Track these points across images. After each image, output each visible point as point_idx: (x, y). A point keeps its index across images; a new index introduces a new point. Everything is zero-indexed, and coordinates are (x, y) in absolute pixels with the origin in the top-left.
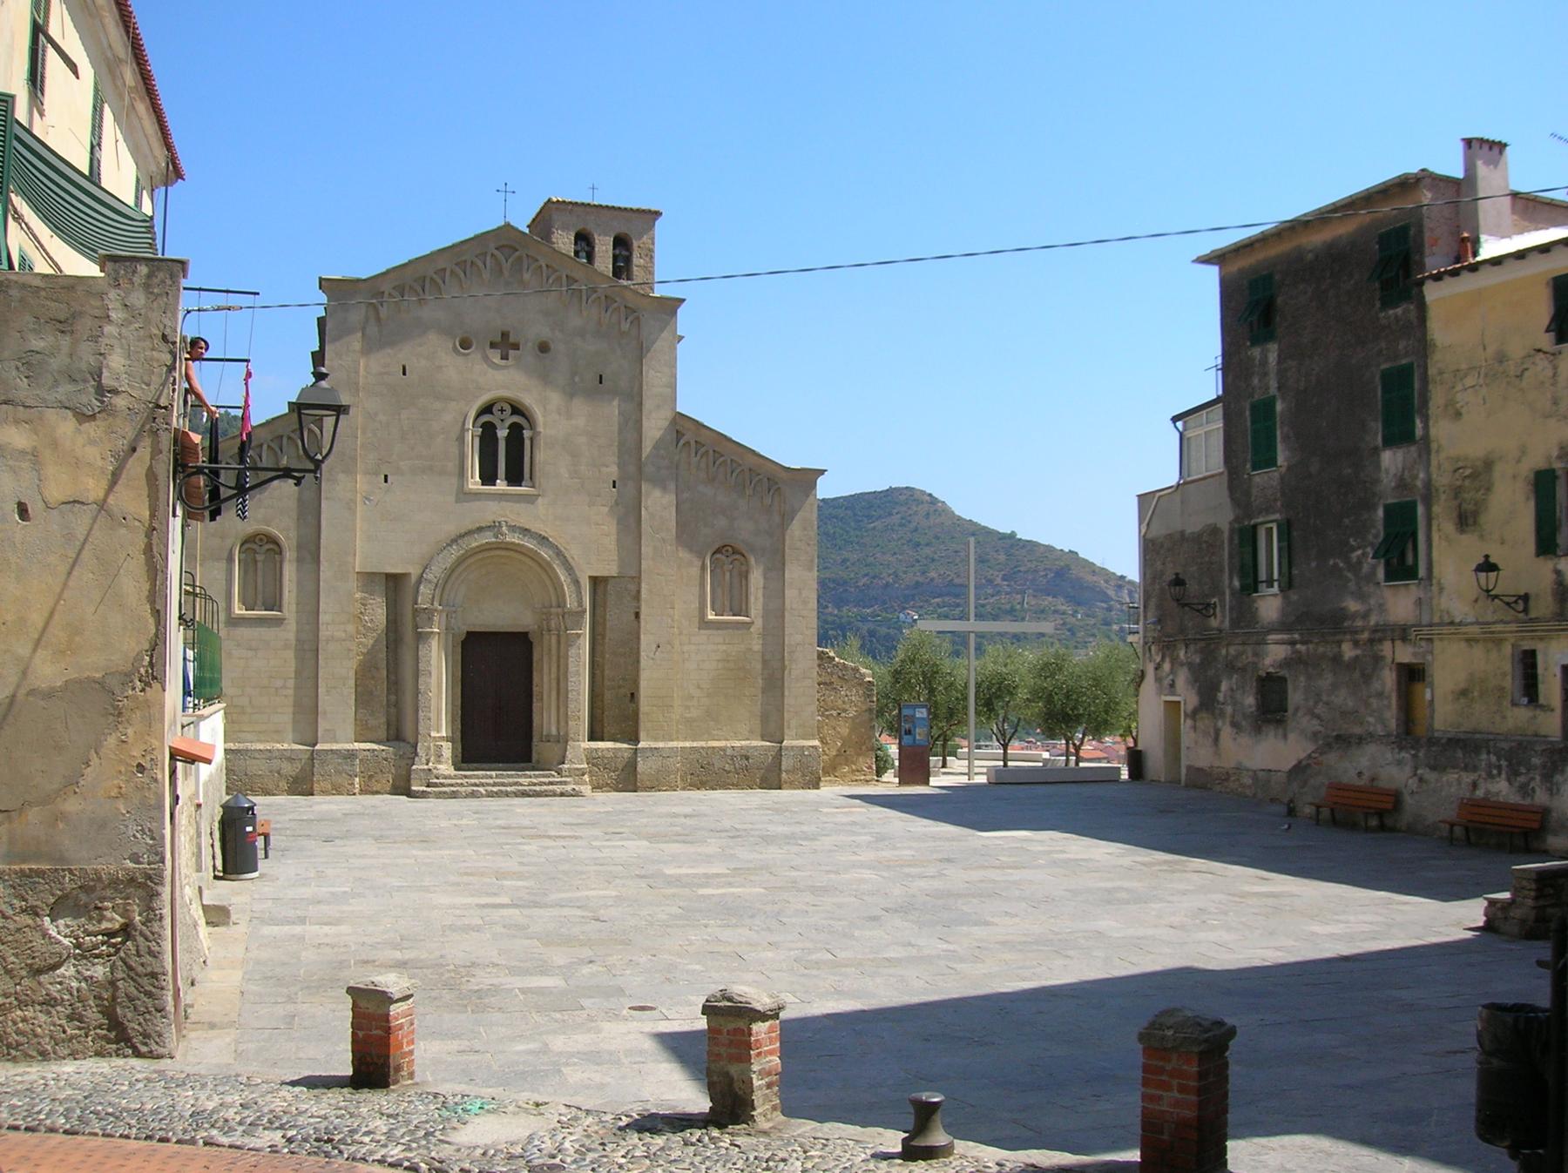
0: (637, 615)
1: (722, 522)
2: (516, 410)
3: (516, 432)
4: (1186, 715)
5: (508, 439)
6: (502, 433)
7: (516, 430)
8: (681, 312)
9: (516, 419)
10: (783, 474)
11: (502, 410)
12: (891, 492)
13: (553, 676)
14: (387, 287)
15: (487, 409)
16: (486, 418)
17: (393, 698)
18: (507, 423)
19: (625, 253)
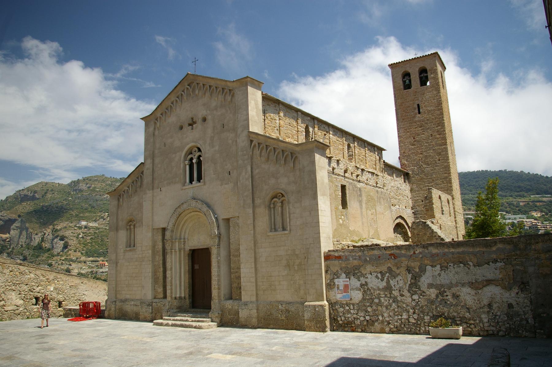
19: (425, 75)
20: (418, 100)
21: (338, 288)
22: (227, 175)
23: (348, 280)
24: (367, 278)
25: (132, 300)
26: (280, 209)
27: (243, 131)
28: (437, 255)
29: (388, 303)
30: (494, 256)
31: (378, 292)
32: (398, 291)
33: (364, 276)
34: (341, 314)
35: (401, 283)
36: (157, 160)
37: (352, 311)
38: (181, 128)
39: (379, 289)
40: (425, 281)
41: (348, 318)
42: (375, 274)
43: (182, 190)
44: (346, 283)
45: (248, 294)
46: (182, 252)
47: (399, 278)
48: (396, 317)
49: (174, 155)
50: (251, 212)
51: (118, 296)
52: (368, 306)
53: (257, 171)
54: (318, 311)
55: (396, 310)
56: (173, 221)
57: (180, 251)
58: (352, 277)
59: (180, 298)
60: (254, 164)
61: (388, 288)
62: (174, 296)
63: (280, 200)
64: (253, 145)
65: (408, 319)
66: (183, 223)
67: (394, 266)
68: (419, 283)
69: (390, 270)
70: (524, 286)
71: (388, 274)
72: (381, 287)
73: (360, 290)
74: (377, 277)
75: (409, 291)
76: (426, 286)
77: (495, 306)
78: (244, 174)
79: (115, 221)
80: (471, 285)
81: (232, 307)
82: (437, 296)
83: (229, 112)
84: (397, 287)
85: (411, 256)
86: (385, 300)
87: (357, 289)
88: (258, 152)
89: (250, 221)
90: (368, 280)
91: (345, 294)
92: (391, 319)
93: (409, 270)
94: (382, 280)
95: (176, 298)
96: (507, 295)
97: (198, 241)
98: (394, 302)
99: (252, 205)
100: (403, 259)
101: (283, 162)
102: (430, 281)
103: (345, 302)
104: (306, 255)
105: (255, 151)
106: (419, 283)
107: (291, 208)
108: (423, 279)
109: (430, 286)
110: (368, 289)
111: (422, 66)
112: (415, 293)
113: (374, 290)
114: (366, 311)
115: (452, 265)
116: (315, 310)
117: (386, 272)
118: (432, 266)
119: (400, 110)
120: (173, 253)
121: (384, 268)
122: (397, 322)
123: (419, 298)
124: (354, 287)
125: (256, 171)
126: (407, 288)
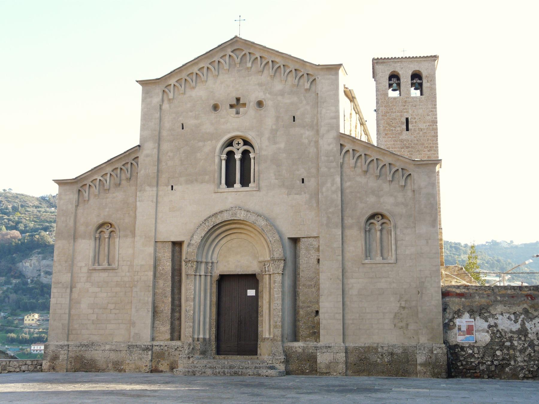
1: (372, 199)
4: (22, 349)
6: (238, 156)
7: (245, 153)
8: (341, 71)
9: (247, 147)
11: (238, 144)
15: (230, 143)
17: (177, 315)
18: (241, 150)
19: (419, 81)
20: (407, 112)
21: (459, 329)
22: (299, 182)
23: (473, 320)
24: (497, 319)
27: (328, 131)
29: (523, 346)
31: (510, 335)
32: (535, 335)
34: (462, 359)
36: (165, 146)
37: (476, 355)
38: (216, 107)
39: (511, 332)
41: (472, 362)
42: (508, 315)
45: (330, 335)
48: (532, 363)
49: (201, 144)
52: (498, 350)
53: (348, 184)
54: (436, 354)
55: (532, 354)
58: (478, 317)
59: (204, 339)
60: (344, 174)
61: (523, 332)
62: (196, 337)
64: (344, 151)
67: (530, 307)
69: (526, 312)
71: (523, 316)
73: (488, 332)
78: (329, 185)
79: (71, 223)
81: (303, 350)
83: (304, 102)
86: (518, 343)
87: (483, 331)
88: (353, 162)
89: (338, 244)
90: (499, 322)
91: (468, 336)
92: (526, 364)
95: (198, 339)
98: (529, 345)
99: (340, 225)
101: (389, 178)
103: (467, 345)
104: (419, 290)
105: (346, 159)
107: (398, 233)
110: (498, 331)
111: (418, 69)
113: (505, 332)
114: (494, 355)
116: (432, 353)
119: (382, 122)
121: (519, 309)
122: (532, 367)
124: (480, 329)
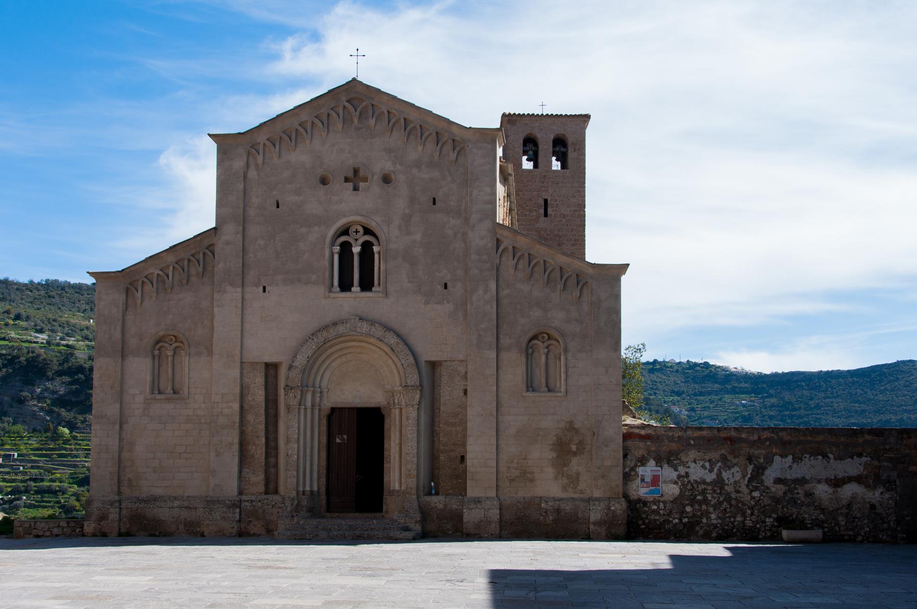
0: (465, 392)
1: (537, 313)
2: (367, 231)
3: (367, 247)
5: (361, 254)
6: (356, 250)
9: (368, 238)
10: (590, 271)
11: (357, 232)
12: (898, 364)
13: (397, 442)
14: (262, 138)
16: (343, 239)
18: (361, 241)
22: (440, 288)
23: (659, 468)
25: (176, 498)
26: (543, 358)
28: (790, 443)
30: (860, 449)
31: (703, 486)
33: (684, 464)
35: (738, 476)
36: (253, 231)
37: (661, 512)
40: (770, 475)
42: (702, 463)
43: (326, 298)
44: (656, 473)
46: (316, 411)
47: (736, 469)
50: (495, 356)
51: (126, 490)
56: (308, 351)
57: (313, 409)
58: (666, 466)
63: (546, 344)
65: (743, 522)
66: (324, 356)
68: (764, 477)
70: (889, 485)
71: (720, 464)
72: (708, 480)
73: (676, 483)
74: (703, 467)
75: (747, 486)
76: (772, 481)
77: (855, 507)
79: (117, 334)
80: (828, 481)
82: (785, 493)
84: (732, 481)
85: (755, 441)
86: (712, 497)
90: (691, 471)
93: (750, 459)
94: (711, 471)
96: (870, 494)
97: (356, 393)
100: (745, 445)
101: (560, 286)
102: (777, 474)
105: (504, 259)
106: (764, 477)
107: (569, 358)
108: (767, 472)
109: (778, 481)
112: (756, 489)
115: (808, 456)
117: (718, 461)
118: (782, 456)
120: (302, 411)
123: (761, 495)
125: (504, 292)
126: (746, 482)
